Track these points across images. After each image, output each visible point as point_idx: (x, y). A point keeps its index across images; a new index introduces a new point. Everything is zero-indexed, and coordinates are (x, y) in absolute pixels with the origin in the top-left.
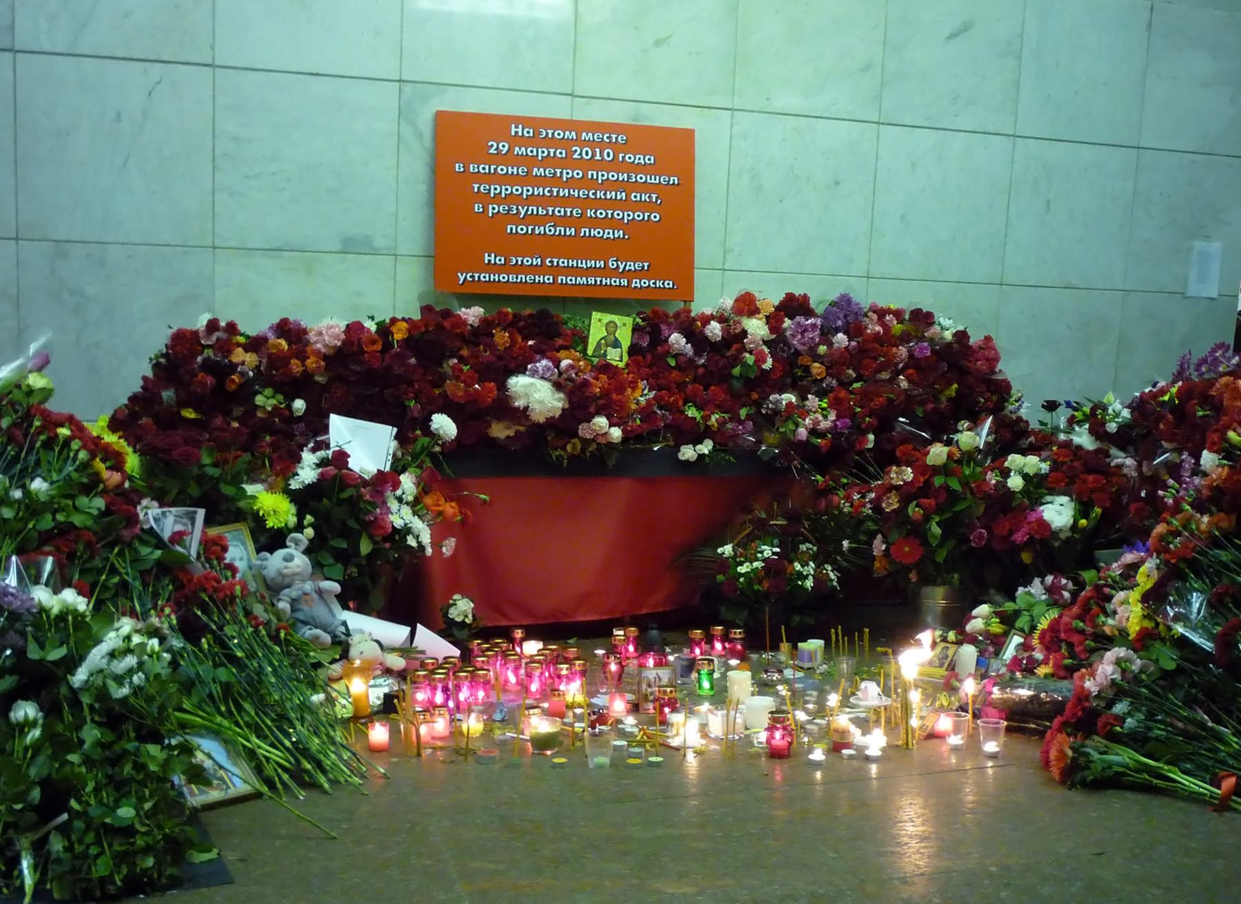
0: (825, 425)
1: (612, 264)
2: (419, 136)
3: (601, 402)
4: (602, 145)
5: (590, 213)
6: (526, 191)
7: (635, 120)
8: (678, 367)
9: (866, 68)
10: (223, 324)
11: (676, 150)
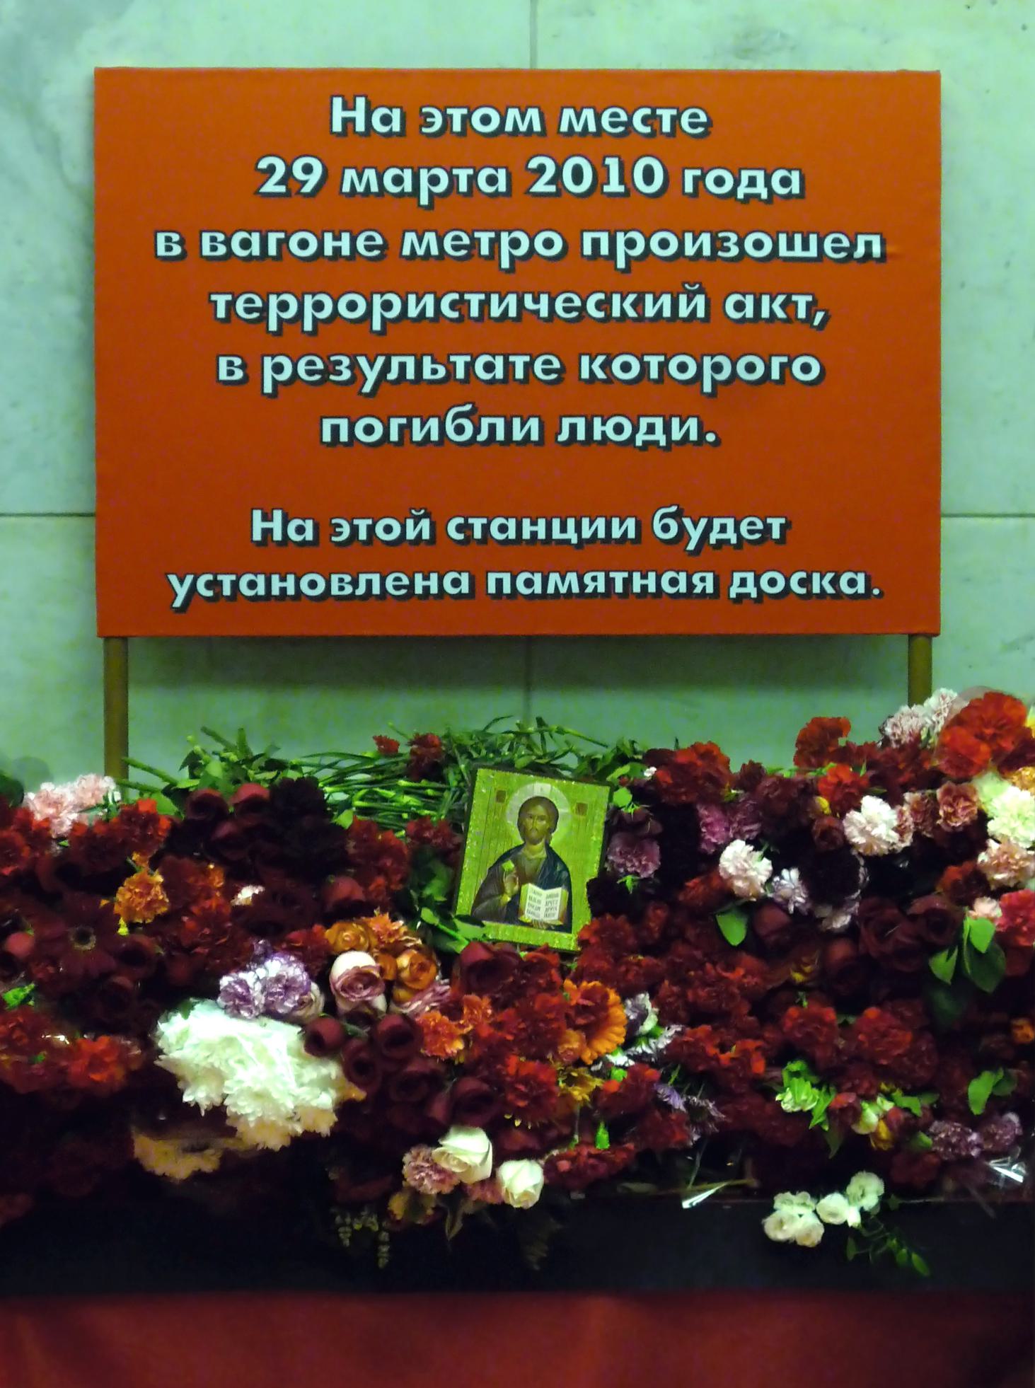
1: (662, 527)
2: (52, 147)
3: (470, 1084)
4: (626, 143)
7: (745, 52)
8: (753, 943)
11: (875, 143)
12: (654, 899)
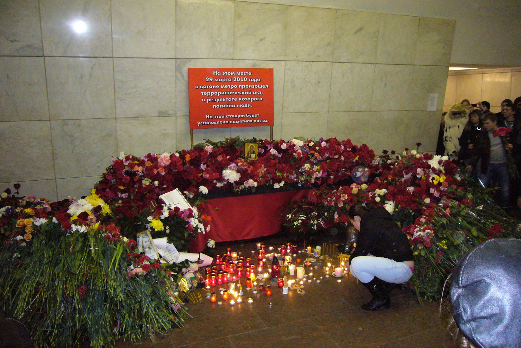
0: (319, 175)
1: (247, 116)
2: (183, 76)
4: (243, 76)
5: (240, 99)
6: (219, 94)
9: (329, 44)
10: (131, 157)
11: (267, 75)
12: (264, 156)
